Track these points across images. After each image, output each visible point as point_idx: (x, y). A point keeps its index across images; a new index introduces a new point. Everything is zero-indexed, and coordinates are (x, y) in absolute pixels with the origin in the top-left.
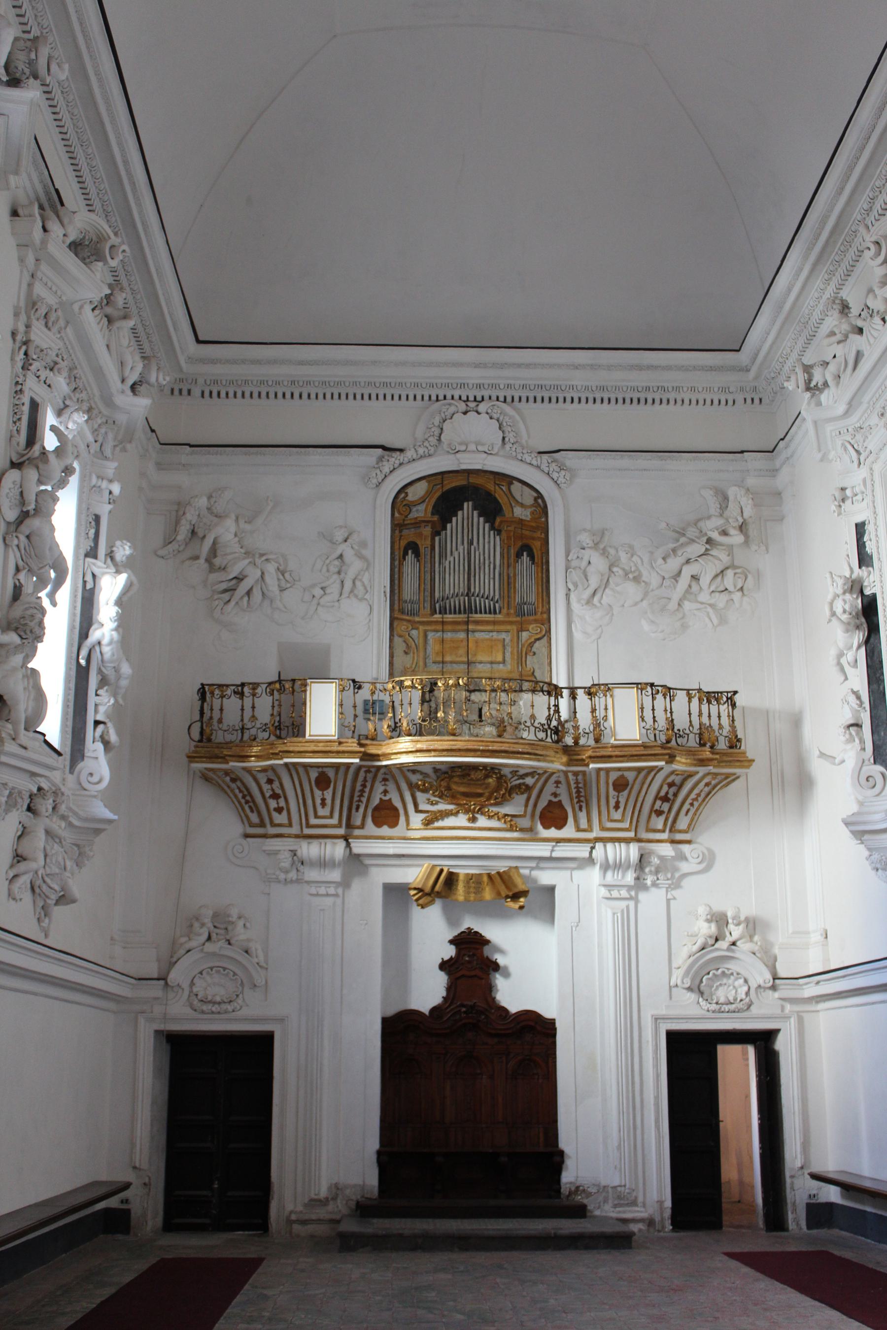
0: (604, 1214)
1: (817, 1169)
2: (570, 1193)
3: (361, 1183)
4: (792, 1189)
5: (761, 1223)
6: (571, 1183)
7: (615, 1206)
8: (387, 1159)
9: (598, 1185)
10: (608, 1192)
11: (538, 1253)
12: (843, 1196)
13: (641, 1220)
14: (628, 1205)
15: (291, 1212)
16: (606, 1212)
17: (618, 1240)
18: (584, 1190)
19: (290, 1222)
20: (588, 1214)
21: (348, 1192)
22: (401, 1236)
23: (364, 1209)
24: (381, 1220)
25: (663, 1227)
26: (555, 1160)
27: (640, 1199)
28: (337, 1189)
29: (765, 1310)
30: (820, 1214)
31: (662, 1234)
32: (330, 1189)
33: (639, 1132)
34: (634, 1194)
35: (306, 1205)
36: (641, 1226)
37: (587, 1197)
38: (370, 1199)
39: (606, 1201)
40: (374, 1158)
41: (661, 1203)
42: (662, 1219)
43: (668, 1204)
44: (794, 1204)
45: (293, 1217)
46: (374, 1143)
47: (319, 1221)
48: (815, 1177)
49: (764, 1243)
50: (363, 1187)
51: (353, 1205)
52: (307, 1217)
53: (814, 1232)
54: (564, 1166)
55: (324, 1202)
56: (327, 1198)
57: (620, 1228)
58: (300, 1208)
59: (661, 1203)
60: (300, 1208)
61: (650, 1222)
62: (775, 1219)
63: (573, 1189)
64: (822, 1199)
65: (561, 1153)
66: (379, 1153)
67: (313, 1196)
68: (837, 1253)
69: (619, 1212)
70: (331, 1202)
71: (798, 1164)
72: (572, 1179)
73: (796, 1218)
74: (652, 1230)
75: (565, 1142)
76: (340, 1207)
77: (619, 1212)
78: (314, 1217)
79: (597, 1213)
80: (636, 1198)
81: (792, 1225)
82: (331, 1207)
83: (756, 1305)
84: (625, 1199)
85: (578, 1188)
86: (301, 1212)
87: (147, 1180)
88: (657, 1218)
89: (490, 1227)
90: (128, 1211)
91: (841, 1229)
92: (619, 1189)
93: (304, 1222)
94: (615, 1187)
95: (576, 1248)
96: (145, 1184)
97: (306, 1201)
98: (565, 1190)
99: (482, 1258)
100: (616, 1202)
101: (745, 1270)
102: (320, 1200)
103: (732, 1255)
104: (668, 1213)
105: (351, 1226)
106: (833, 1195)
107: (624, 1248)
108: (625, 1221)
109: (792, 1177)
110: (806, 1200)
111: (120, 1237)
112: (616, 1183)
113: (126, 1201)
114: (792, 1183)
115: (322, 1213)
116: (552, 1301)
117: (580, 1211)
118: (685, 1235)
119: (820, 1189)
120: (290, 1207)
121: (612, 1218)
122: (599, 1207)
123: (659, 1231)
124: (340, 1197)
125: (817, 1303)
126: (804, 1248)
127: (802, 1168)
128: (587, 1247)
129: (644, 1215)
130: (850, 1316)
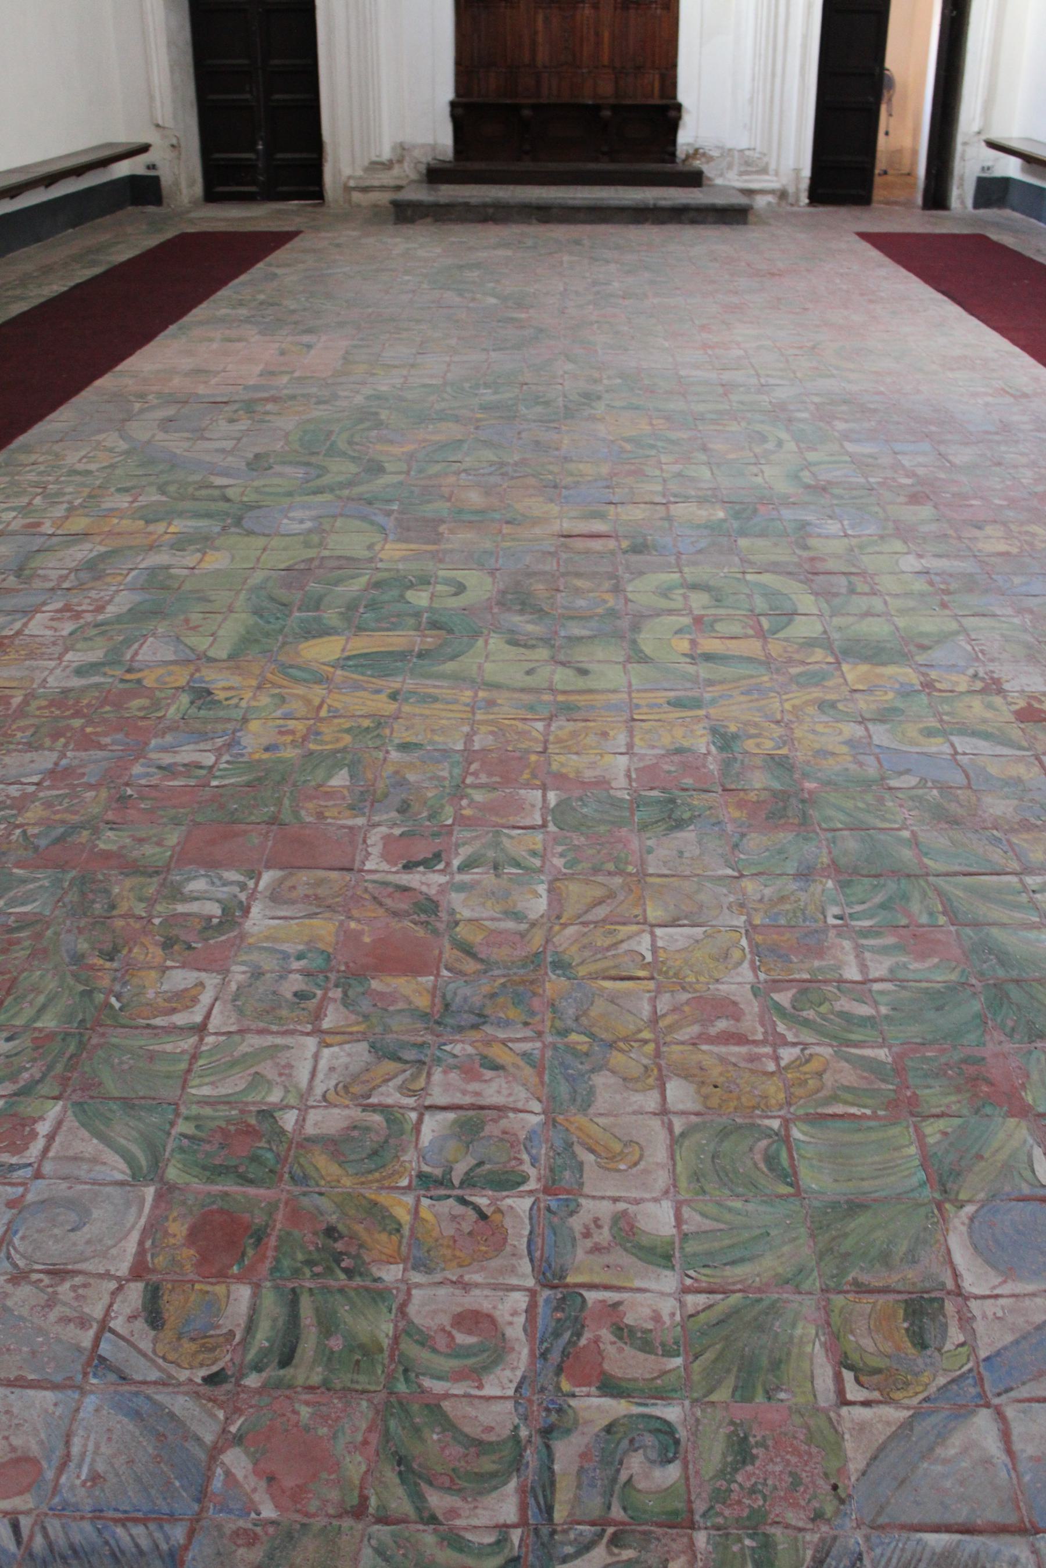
0: (727, 183)
1: (997, 135)
2: (688, 157)
3: (432, 142)
4: (963, 159)
5: (919, 200)
6: (689, 144)
7: (741, 174)
8: (465, 114)
9: (722, 148)
10: (733, 157)
11: (631, 227)
12: (1024, 170)
13: (772, 192)
14: (758, 172)
15: (349, 178)
16: (726, 182)
17: (733, 215)
18: (704, 154)
19: (348, 189)
20: (705, 182)
21: (416, 153)
22: (467, 205)
23: (435, 175)
24: (452, 187)
25: (797, 200)
26: (666, 116)
27: (772, 166)
28: (402, 150)
29: (871, 301)
30: (992, 191)
31: (795, 209)
32: (394, 149)
33: (778, 81)
34: (765, 160)
35: (366, 170)
36: (770, 198)
37: (708, 162)
38: (444, 162)
39: (730, 166)
40: (446, 110)
41: (797, 171)
42: (798, 189)
43: (807, 172)
44: (962, 178)
45: (352, 183)
46: (446, 92)
47: (383, 188)
48: (992, 145)
49: (916, 222)
50: (434, 147)
51: (423, 168)
52: (367, 183)
53: (981, 212)
54: (681, 123)
55: (388, 166)
56: (391, 161)
57: (743, 200)
58: (359, 173)
59: (797, 171)
60: (359, 173)
61: (783, 195)
62: (936, 195)
63: (691, 151)
64: (999, 172)
65: (679, 107)
66: (453, 105)
67: (375, 159)
68: (994, 237)
69: (746, 181)
70: (396, 166)
71: (975, 128)
72: (690, 140)
73: (961, 194)
74: (783, 203)
75: (684, 95)
76: (408, 171)
77: (746, 181)
78: (376, 183)
79: (719, 181)
80: (767, 164)
81: (954, 202)
82: (396, 171)
83: (862, 295)
84: (751, 165)
85: (696, 150)
86: (361, 178)
87: (174, 142)
88: (791, 190)
89: (579, 195)
90: (156, 180)
91: (1014, 209)
92: (747, 153)
93: (365, 190)
94: (741, 151)
95: (680, 222)
96: (173, 146)
97: (366, 163)
98: (681, 150)
99: (560, 232)
100: (743, 169)
101: (875, 254)
102: (382, 164)
103: (864, 236)
104: (805, 184)
105: (422, 194)
106: (1011, 168)
107: (738, 223)
108: (750, 192)
109: (965, 144)
110: (978, 173)
111: (151, 209)
112: (744, 145)
113: (152, 167)
114: (964, 151)
115: (386, 178)
116: (616, 284)
117: (695, 179)
118: (823, 211)
119: (997, 159)
120: (347, 171)
121: (734, 188)
122: (721, 175)
123: (792, 205)
124: (407, 158)
125: (939, 296)
126: (965, 231)
127: (979, 133)
128: (693, 222)
129: (776, 185)
130: (972, 314)
